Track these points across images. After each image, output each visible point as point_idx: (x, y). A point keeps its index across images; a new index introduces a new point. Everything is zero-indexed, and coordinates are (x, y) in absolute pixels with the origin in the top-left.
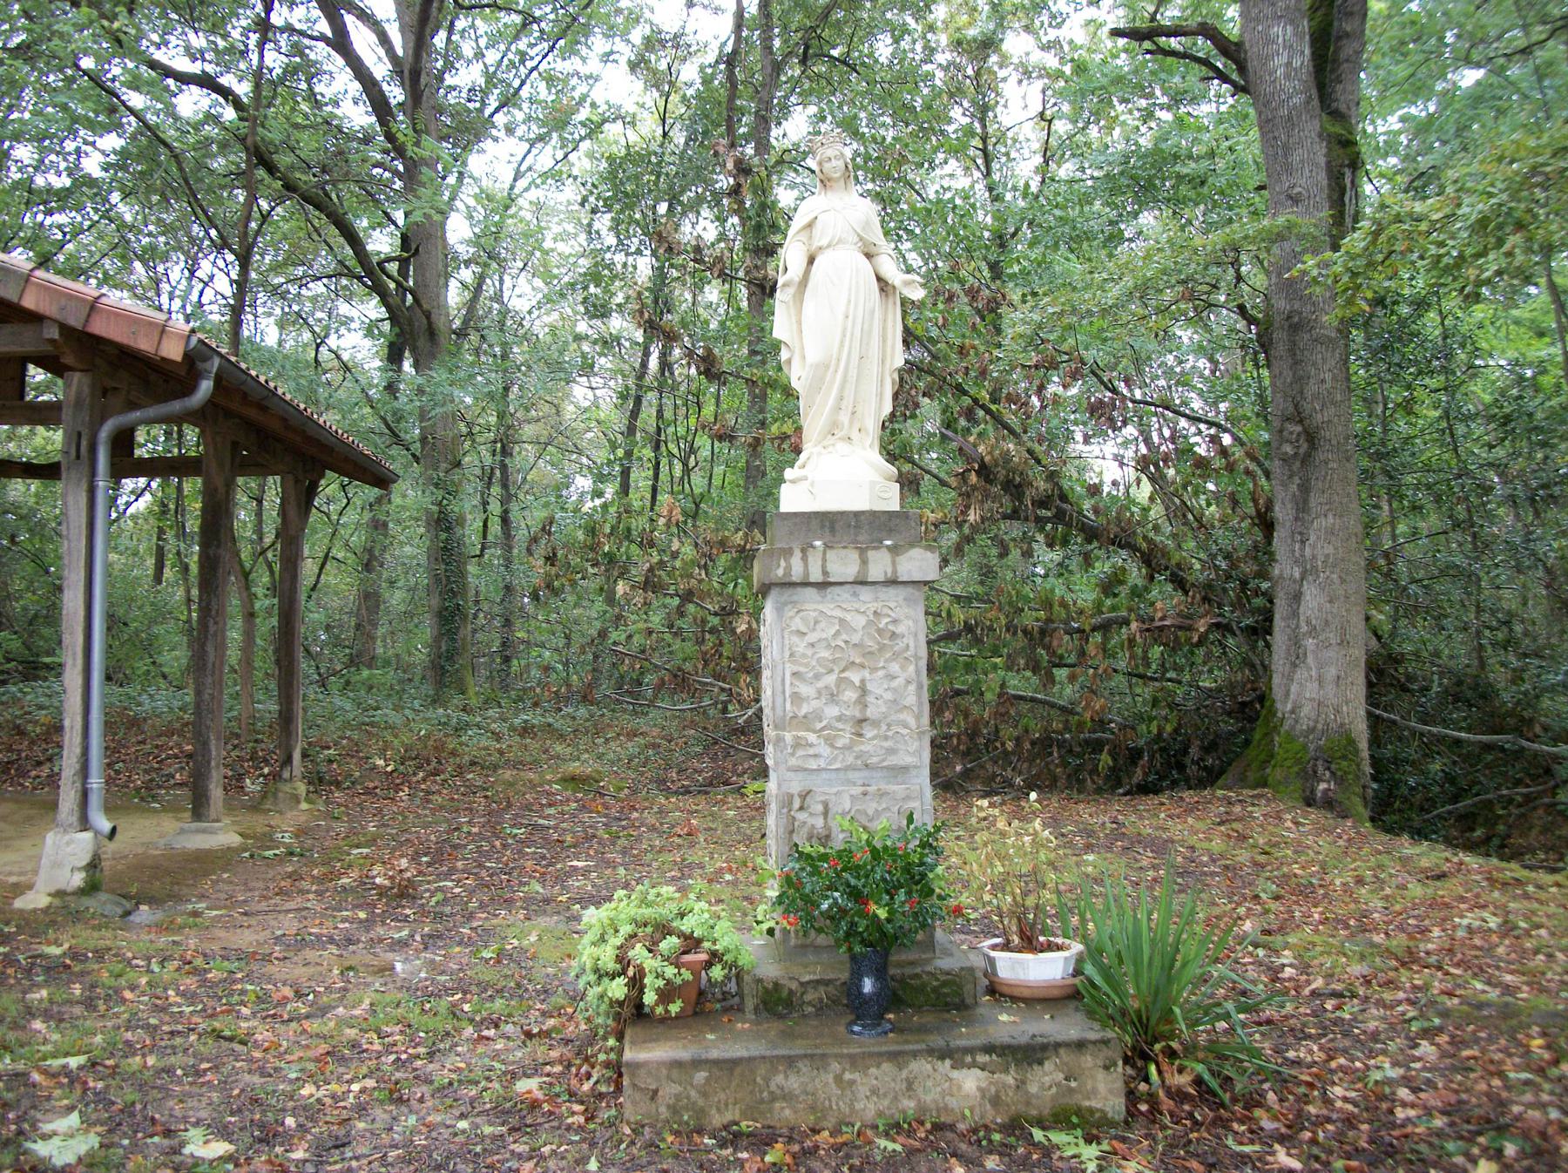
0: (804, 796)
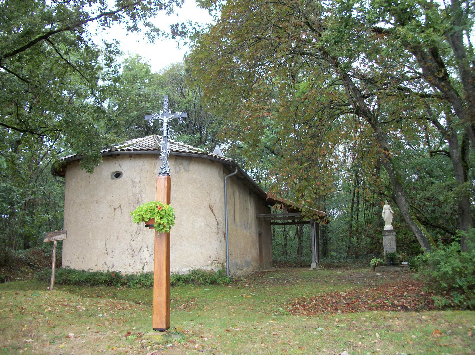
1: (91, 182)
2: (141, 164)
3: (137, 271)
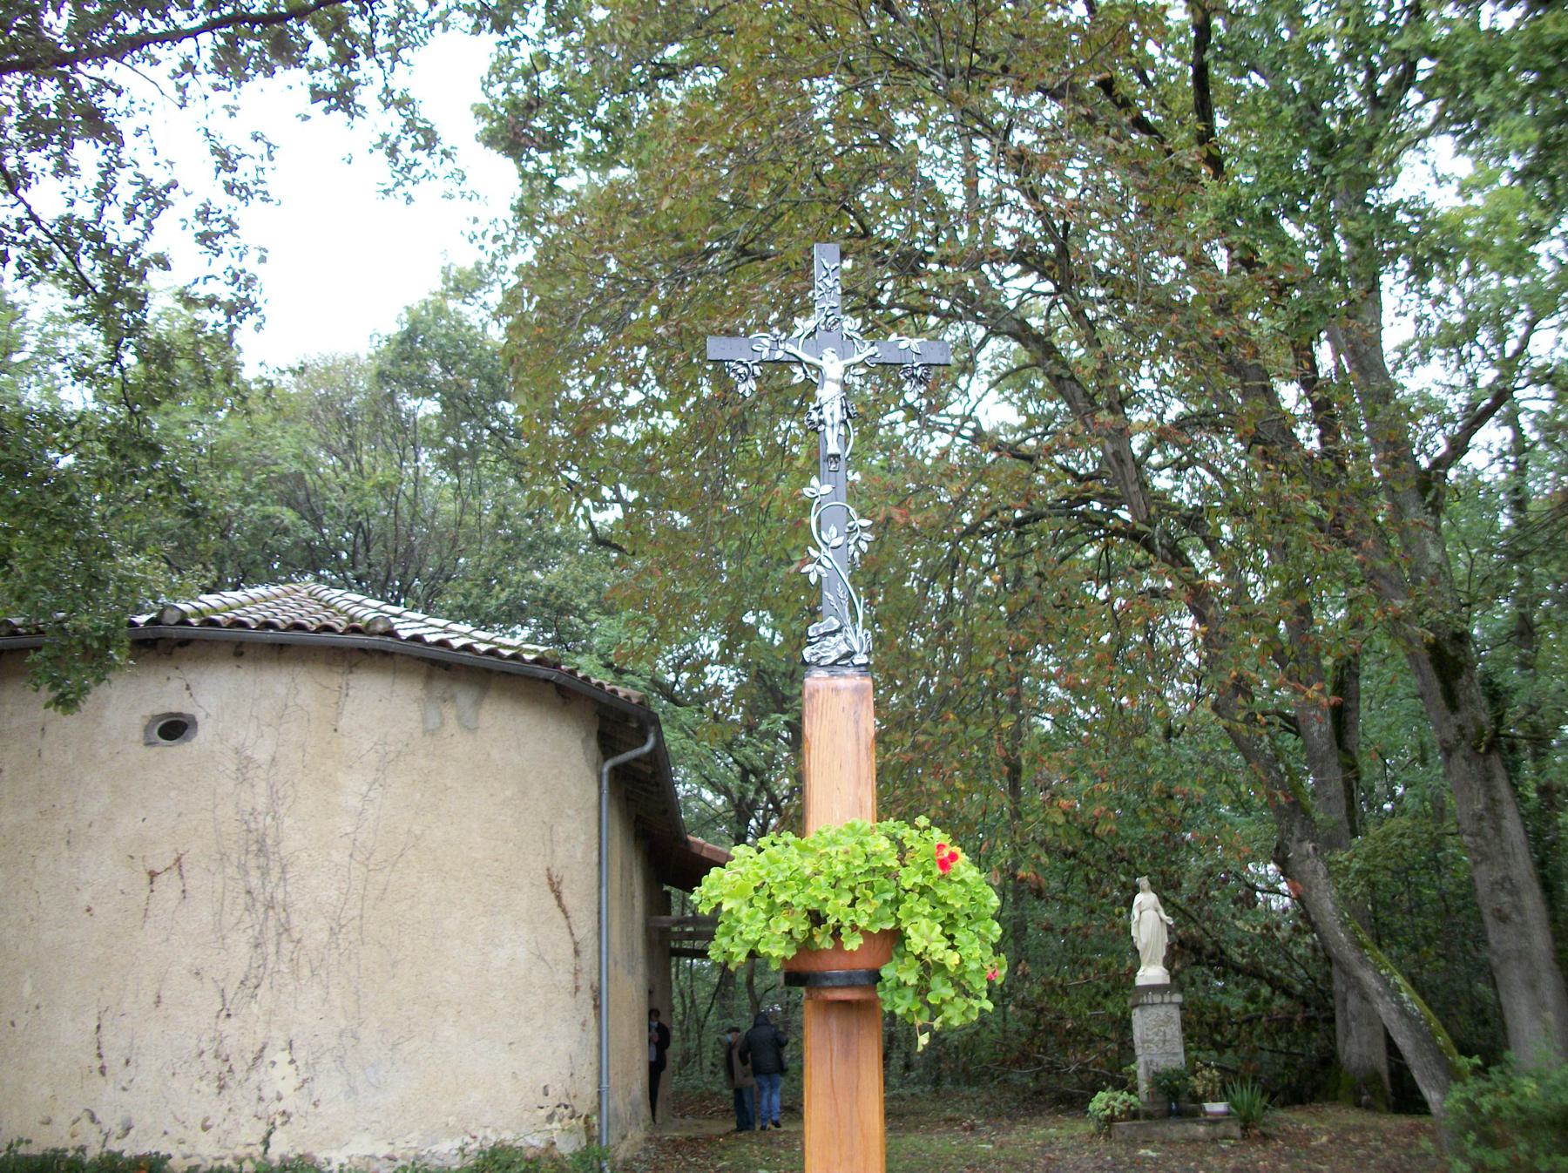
1: (46, 754)
2: (282, 690)
3: (241, 1152)
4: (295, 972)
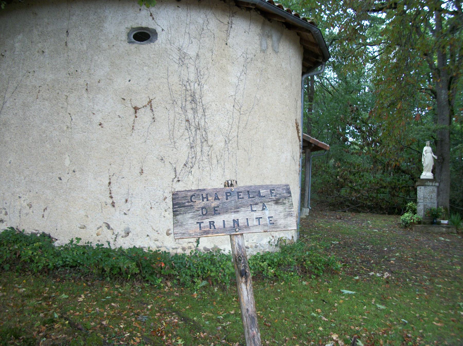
0: (426, 205)
1: (70, 45)
2: (200, 21)
4: (210, 161)
